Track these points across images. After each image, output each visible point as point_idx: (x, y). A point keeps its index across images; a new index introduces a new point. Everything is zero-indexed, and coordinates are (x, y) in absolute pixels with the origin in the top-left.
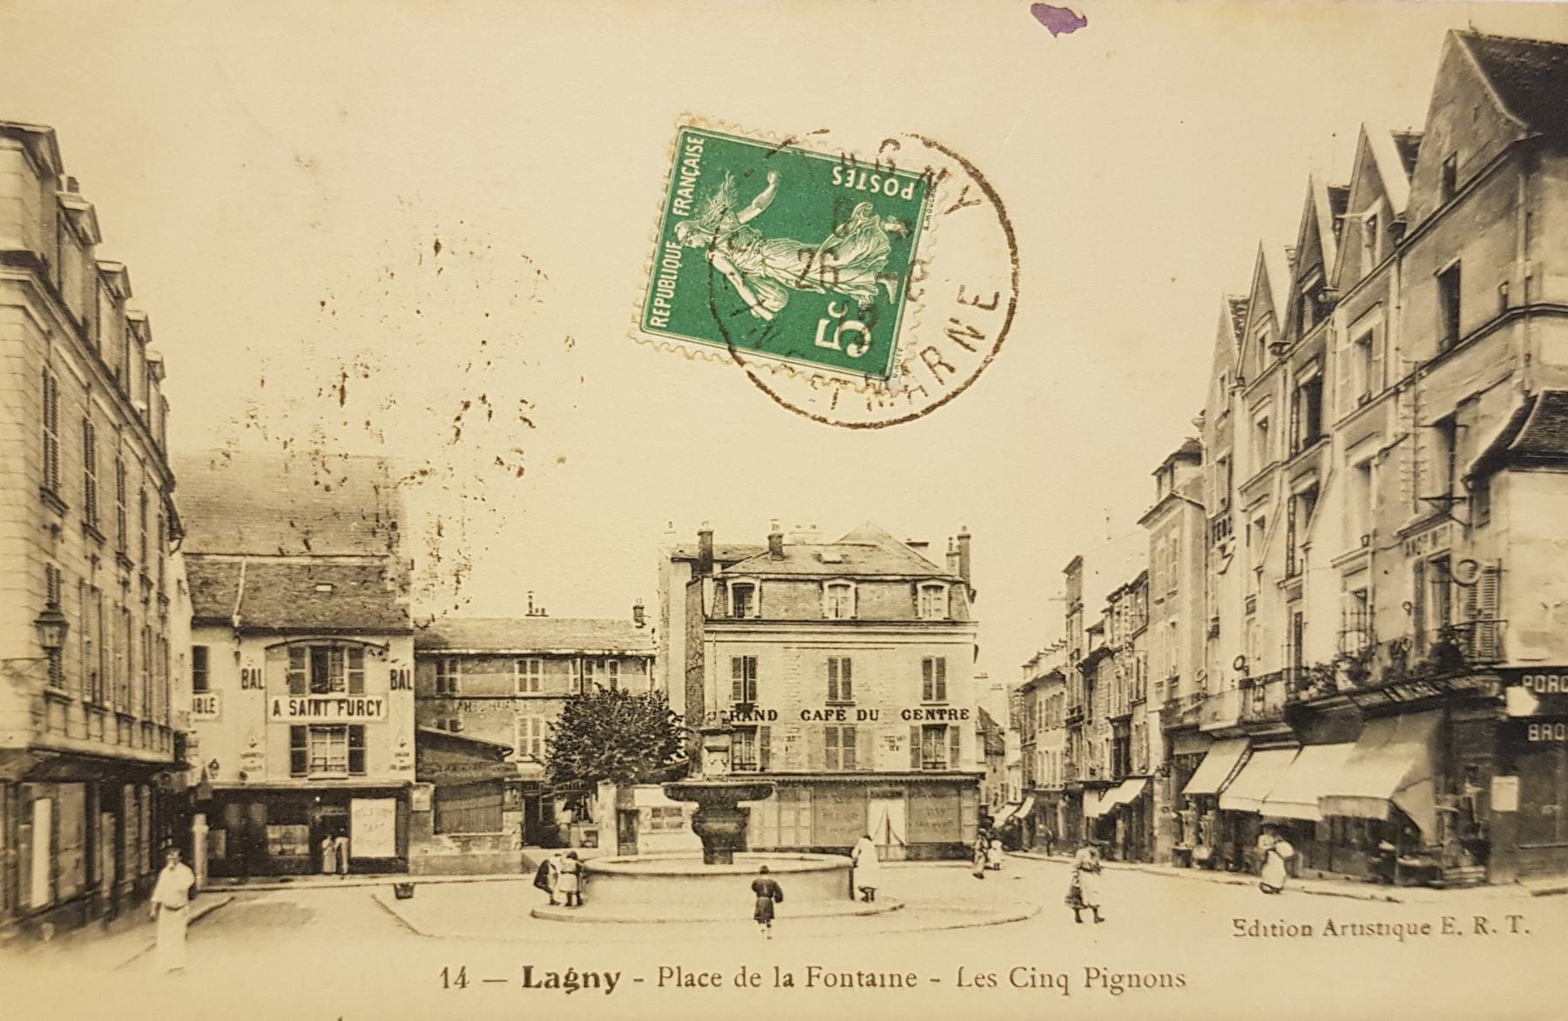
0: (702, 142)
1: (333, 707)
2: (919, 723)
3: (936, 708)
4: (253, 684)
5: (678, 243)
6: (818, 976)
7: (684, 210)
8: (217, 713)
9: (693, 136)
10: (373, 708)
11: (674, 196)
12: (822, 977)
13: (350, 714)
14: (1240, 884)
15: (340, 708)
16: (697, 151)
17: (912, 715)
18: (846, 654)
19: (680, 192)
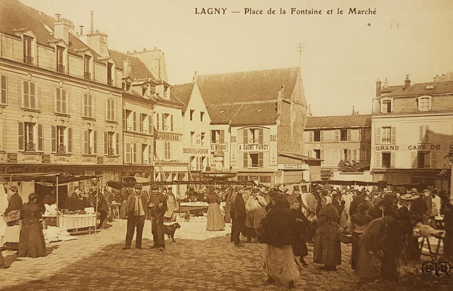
1: (255, 146)
6: (295, 11)
10: (266, 147)
12: (296, 11)
13: (260, 149)
15: (257, 147)
18: (426, 123)
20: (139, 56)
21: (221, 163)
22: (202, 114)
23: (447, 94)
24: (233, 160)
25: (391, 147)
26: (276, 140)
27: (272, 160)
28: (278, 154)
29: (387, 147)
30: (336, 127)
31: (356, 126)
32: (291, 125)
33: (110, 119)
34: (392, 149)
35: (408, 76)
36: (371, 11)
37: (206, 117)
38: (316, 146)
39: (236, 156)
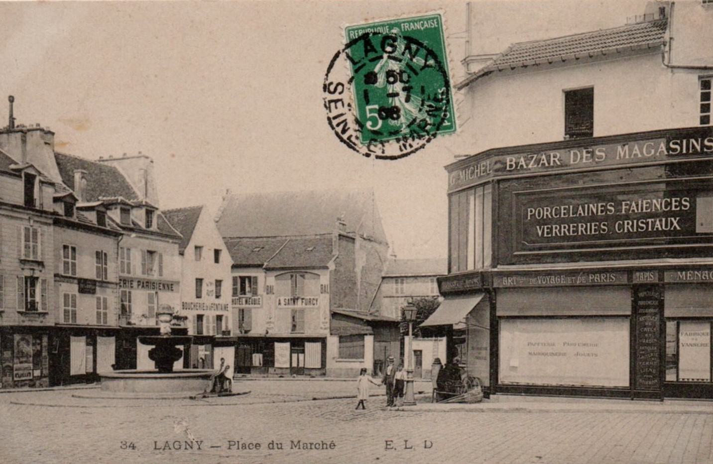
0: (436, 26)
4: (271, 292)
5: (389, 31)
7: (404, 28)
9: (437, 21)
10: (315, 302)
11: (409, 22)
13: (306, 304)
14: (76, 389)
15: (302, 302)
16: (431, 25)
19: (411, 24)
20: (115, 164)
22: (217, 252)
24: (270, 320)
27: (323, 320)
32: (358, 270)
33: (29, 257)
36: (326, 444)
37: (226, 259)
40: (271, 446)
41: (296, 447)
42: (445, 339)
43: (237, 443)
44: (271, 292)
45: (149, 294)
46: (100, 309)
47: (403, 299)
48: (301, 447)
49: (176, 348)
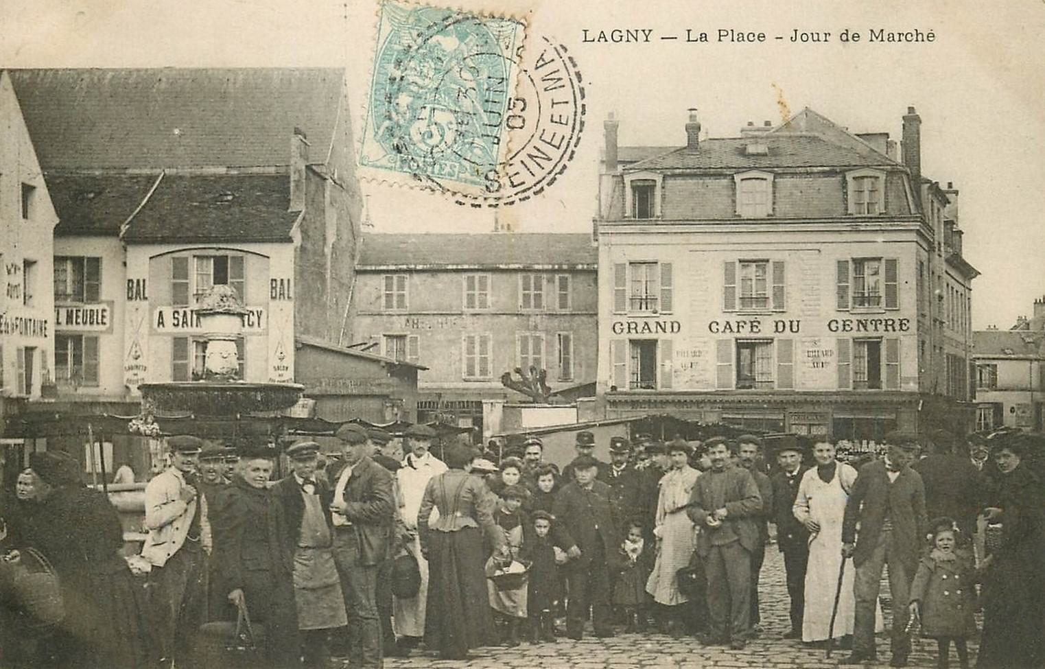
2: (847, 336)
3: (870, 318)
4: (138, 293)
8: (108, 325)
10: (254, 319)
17: (840, 325)
21: (232, 347)
22: (27, 190)
23: (815, 169)
24: (134, 363)
25: (658, 323)
26: (292, 295)
28: (296, 341)
29: (646, 324)
30: (455, 267)
31: (516, 266)
32: (328, 250)
34: (663, 324)
35: (693, 112)
38: (392, 323)
39: (145, 349)
40: (844, 37)
41: (877, 38)
42: (230, 597)
43: (730, 32)
44: (138, 293)
45: (187, 279)
46: (535, 295)
47: (404, 319)
48: (885, 38)
49: (440, 650)
